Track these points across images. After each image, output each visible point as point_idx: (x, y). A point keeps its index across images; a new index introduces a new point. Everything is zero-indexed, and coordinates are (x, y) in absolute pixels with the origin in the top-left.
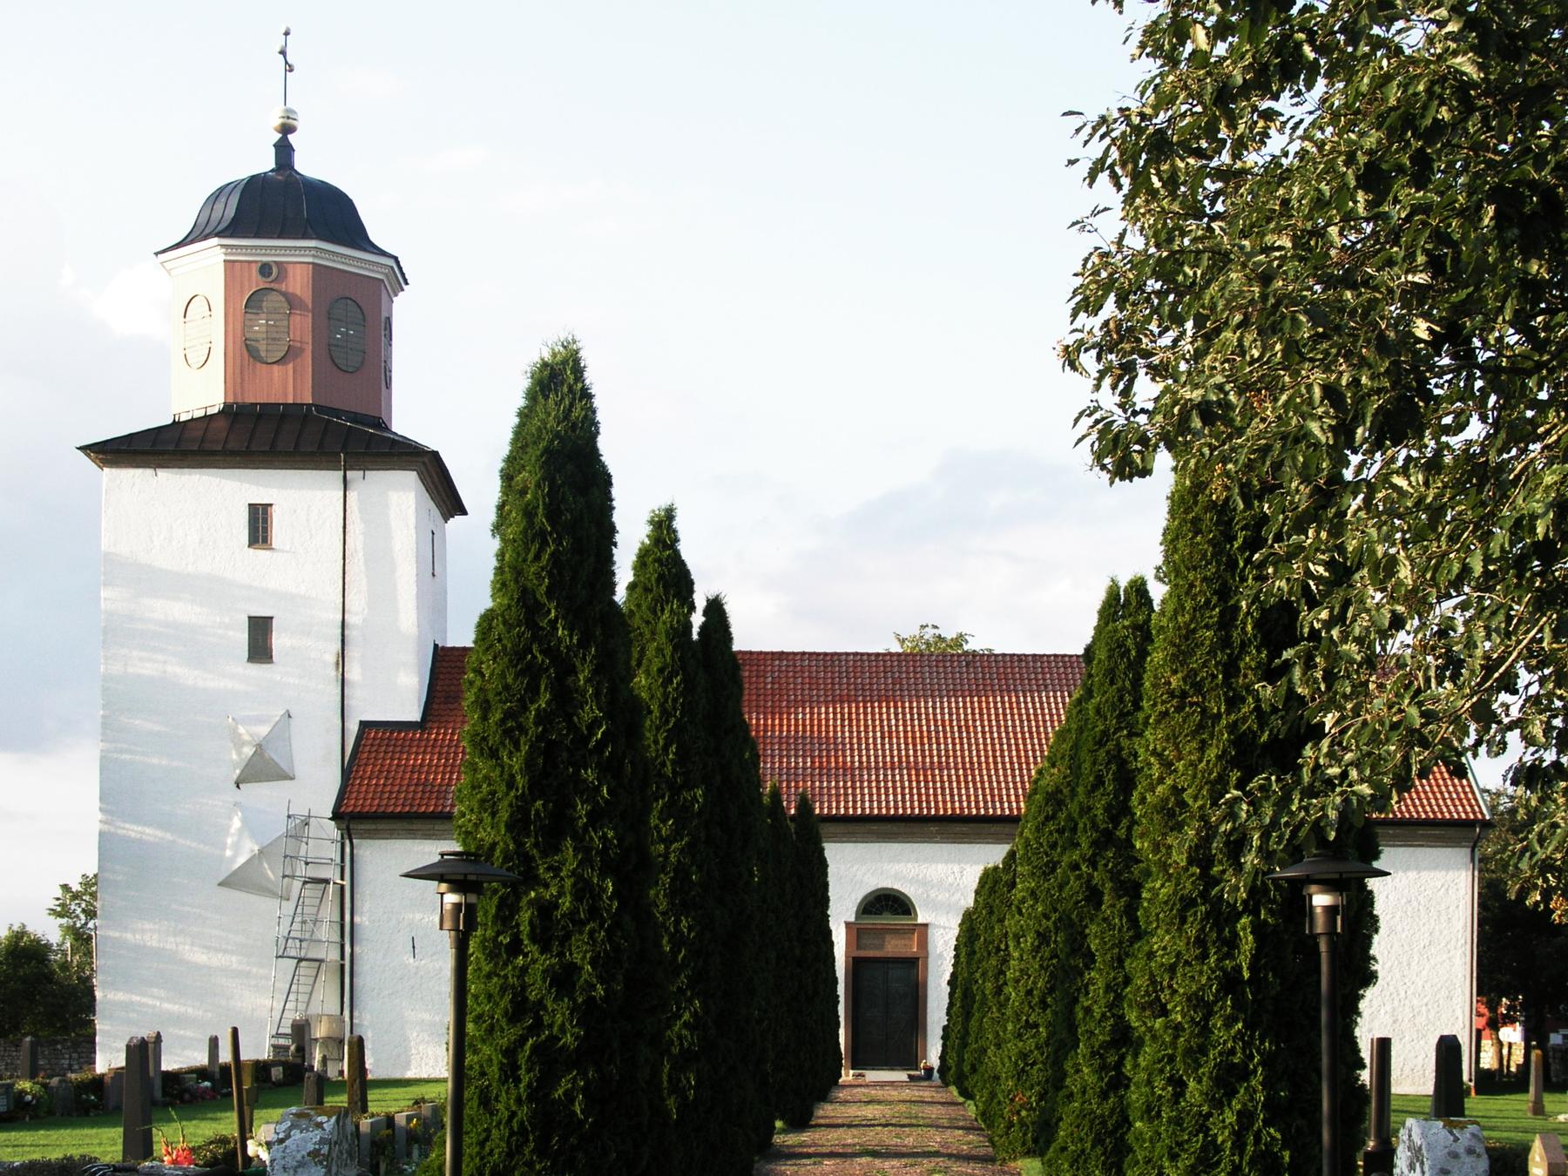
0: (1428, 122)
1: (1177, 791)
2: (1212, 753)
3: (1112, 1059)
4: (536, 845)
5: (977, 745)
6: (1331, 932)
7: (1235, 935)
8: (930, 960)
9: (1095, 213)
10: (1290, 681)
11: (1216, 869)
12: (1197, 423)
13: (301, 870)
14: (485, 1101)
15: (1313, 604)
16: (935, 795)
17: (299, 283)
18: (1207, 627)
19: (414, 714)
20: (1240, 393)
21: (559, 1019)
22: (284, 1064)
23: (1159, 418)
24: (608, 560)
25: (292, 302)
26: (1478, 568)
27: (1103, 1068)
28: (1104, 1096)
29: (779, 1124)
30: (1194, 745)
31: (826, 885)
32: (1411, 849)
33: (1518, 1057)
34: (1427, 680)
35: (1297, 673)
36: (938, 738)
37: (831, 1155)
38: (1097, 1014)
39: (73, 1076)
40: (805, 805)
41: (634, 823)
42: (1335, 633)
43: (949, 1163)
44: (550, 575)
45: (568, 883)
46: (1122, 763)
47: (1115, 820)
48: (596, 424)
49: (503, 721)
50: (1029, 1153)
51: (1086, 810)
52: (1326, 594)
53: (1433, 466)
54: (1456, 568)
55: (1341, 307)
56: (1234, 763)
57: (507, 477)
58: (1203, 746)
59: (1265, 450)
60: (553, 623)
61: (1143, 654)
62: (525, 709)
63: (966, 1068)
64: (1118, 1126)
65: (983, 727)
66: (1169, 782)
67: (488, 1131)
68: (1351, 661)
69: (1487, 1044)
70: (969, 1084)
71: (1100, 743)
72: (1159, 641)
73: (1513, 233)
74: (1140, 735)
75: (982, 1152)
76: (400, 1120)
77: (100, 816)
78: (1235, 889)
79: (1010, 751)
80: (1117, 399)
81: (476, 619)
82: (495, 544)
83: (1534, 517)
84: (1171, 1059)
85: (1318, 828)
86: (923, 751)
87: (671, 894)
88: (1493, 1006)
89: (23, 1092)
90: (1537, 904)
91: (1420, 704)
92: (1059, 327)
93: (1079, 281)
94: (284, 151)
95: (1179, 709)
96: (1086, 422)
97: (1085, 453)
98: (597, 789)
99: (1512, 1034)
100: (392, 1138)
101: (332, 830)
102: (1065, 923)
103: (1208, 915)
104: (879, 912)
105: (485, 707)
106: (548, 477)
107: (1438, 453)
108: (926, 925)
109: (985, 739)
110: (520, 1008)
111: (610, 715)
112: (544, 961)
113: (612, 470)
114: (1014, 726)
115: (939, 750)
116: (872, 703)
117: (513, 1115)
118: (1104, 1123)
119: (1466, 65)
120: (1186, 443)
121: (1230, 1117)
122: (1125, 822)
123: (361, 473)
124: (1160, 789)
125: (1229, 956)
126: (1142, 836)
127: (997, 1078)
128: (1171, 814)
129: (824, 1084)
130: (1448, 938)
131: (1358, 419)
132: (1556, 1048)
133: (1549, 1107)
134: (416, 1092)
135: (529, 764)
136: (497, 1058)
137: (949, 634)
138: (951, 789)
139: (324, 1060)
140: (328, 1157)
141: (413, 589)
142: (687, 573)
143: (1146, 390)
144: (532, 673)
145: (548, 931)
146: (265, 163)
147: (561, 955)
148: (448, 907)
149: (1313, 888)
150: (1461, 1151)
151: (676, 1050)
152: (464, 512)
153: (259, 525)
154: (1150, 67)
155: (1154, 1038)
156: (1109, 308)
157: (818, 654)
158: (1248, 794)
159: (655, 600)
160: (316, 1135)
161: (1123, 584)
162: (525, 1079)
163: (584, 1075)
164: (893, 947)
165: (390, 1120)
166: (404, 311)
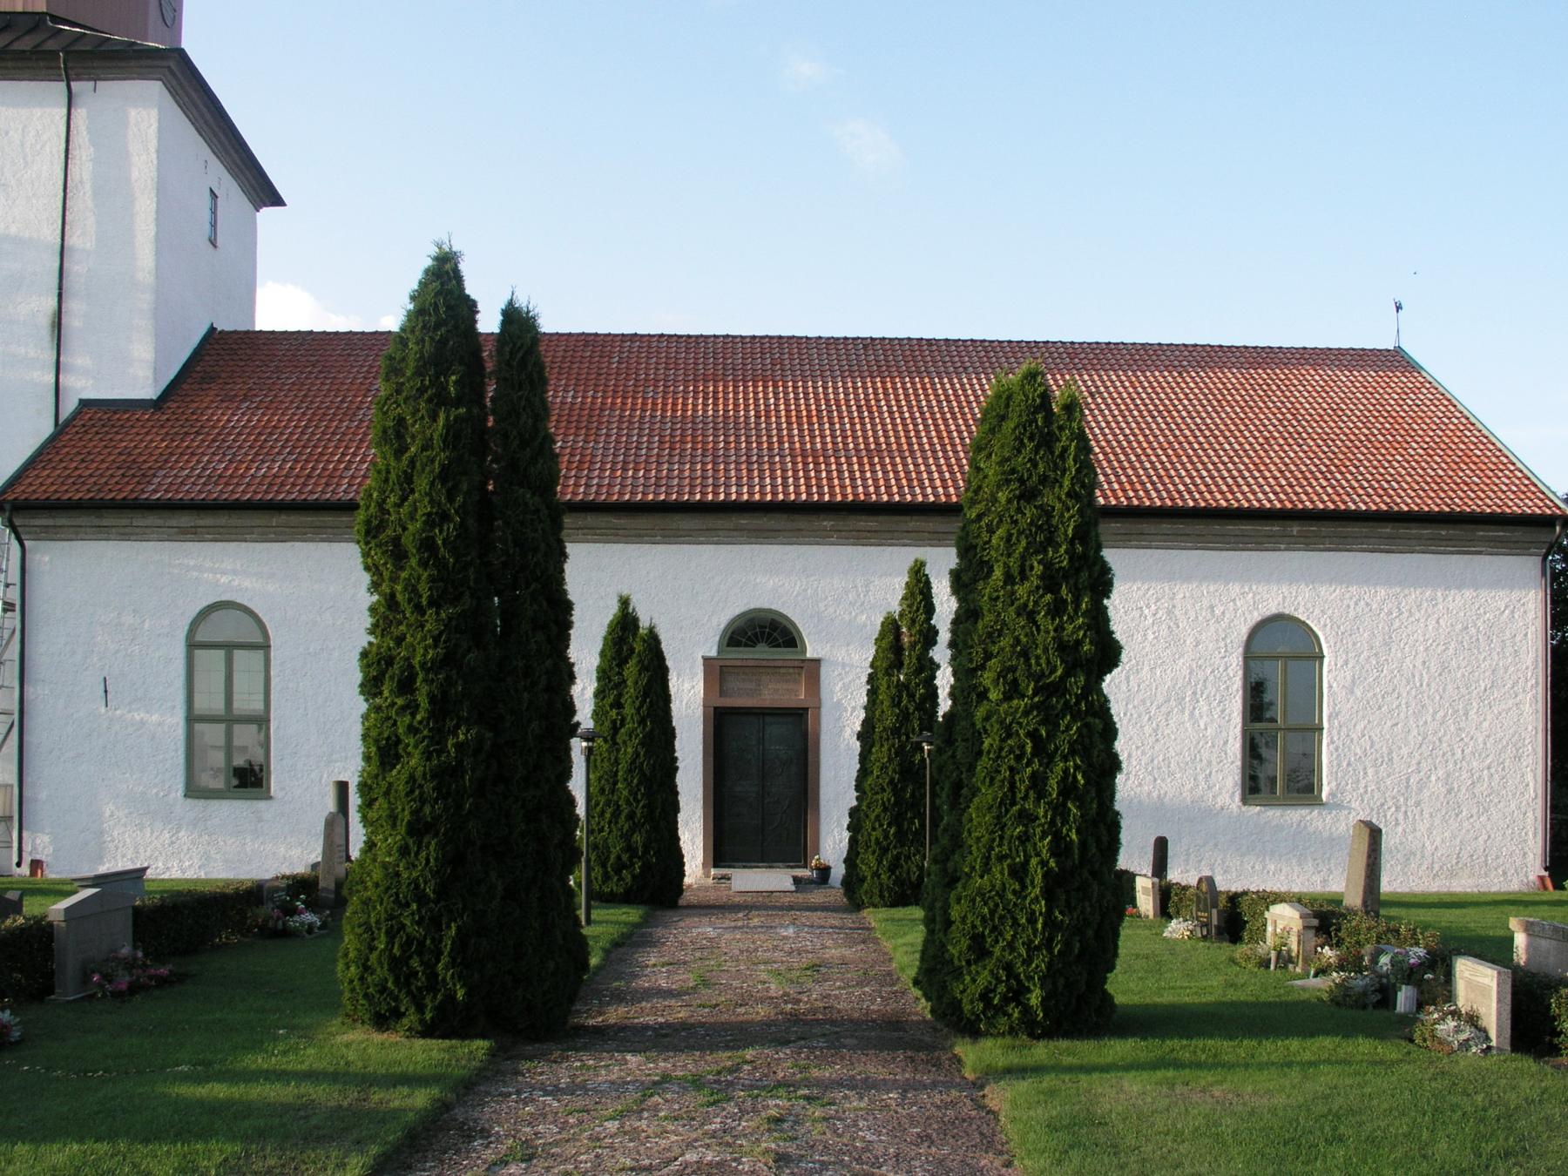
5: (884, 425)
8: (824, 711)
16: (830, 479)
32: (1467, 557)
36: (830, 418)
65: (890, 407)
79: (928, 432)
86: (811, 431)
104: (752, 642)
108: (817, 662)
109: (893, 419)
114: (930, 407)
115: (833, 431)
116: (745, 382)
123: (92, 83)
130: (1514, 677)
138: (851, 472)
152: (277, 201)
157: (681, 337)
164: (772, 694)
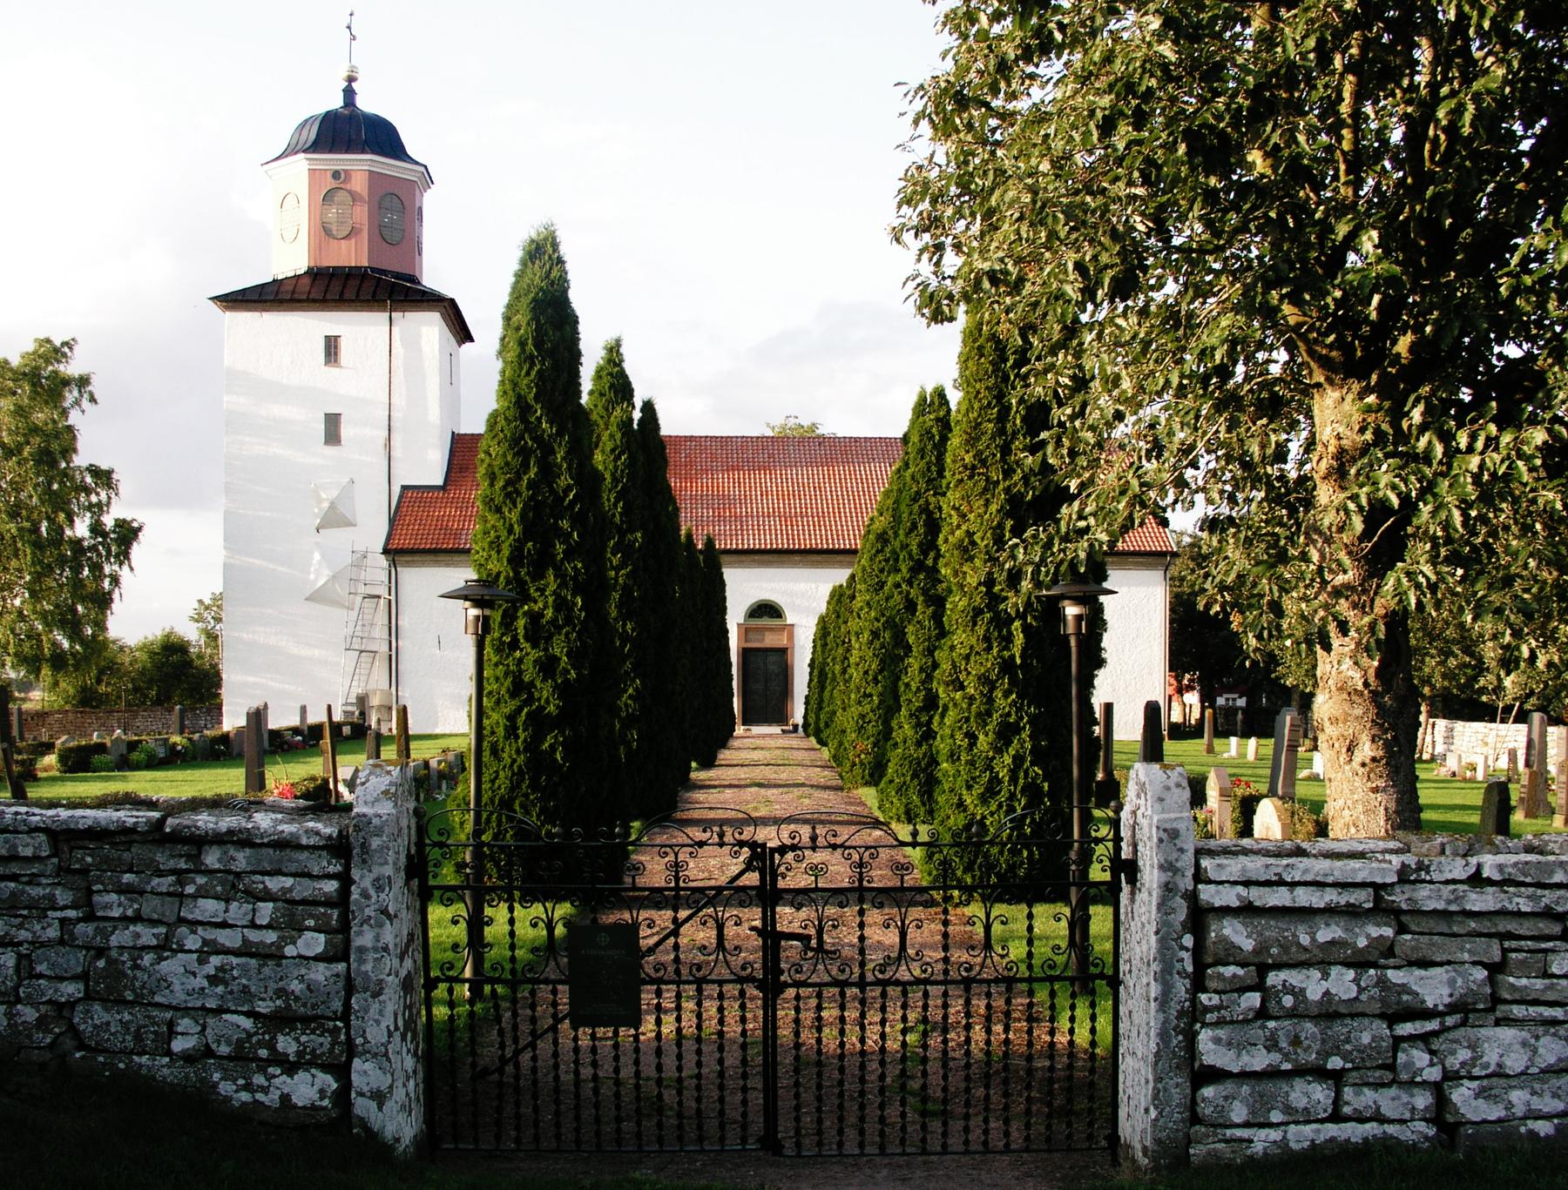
0: (1143, 88)
1: (970, 534)
2: (994, 508)
3: (924, 719)
4: (528, 573)
6: (1078, 633)
7: (1010, 633)
9: (912, 139)
10: (1045, 455)
11: (997, 588)
12: (986, 284)
13: (362, 590)
14: (495, 752)
15: (1061, 404)
17: (359, 184)
18: (989, 421)
19: (439, 481)
20: (1015, 264)
21: (545, 694)
22: (351, 724)
23: (960, 282)
24: (577, 375)
25: (354, 196)
26: (1175, 381)
27: (918, 725)
28: (919, 744)
29: (694, 765)
30: (982, 502)
31: (724, 599)
33: (1196, 714)
34: (1140, 458)
35: (1050, 449)
37: (730, 786)
38: (914, 686)
39: (207, 732)
40: (710, 542)
41: (595, 559)
42: (1077, 423)
43: (811, 791)
44: (537, 385)
45: (551, 599)
46: (930, 514)
47: (925, 554)
48: (566, 281)
49: (504, 487)
50: (867, 784)
51: (904, 546)
52: (1072, 397)
53: (1144, 312)
54: (1161, 382)
55: (1083, 206)
56: (1008, 515)
57: (507, 319)
58: (987, 504)
59: (1035, 305)
60: (539, 419)
61: (944, 439)
62: (520, 479)
63: (822, 725)
64: (929, 765)
66: (964, 527)
67: (497, 772)
68: (1087, 444)
69: (1176, 706)
70: (824, 736)
71: (915, 500)
72: (956, 430)
73: (1198, 160)
74: (944, 494)
75: (834, 783)
76: (433, 764)
77: (224, 552)
78: (1013, 602)
80: (932, 268)
81: (486, 417)
82: (499, 365)
83: (1214, 349)
84: (967, 720)
85: (1073, 565)
87: (619, 607)
88: (1179, 679)
89: (175, 744)
90: (1217, 613)
91: (1139, 477)
92: (889, 215)
93: (903, 183)
94: (349, 93)
95: (971, 477)
96: (913, 284)
97: (911, 306)
98: (570, 535)
99: (1192, 698)
100: (428, 777)
101: (383, 562)
102: (890, 624)
103: (991, 621)
104: (760, 616)
105: (492, 478)
106: (535, 318)
107: (1147, 305)
110: (519, 687)
111: (578, 482)
112: (534, 654)
113: (578, 313)
117: (514, 761)
118: (919, 764)
119: (1167, 50)
120: (980, 299)
121: (1008, 760)
122: (932, 554)
124: (958, 533)
125: (1007, 648)
126: (946, 565)
127: (844, 732)
128: (966, 550)
129: (724, 736)
131: (1099, 283)
132: (1221, 708)
133: (1217, 748)
134: (443, 743)
135: (523, 517)
136: (503, 722)
137: (806, 423)
139: (379, 721)
140: (395, 795)
141: (438, 394)
142: (629, 384)
143: (952, 261)
144: (524, 453)
145: (537, 633)
146: (336, 102)
147: (546, 650)
148: (470, 618)
149: (1066, 602)
150: (1172, 785)
151: (624, 714)
152: (472, 340)
153: (332, 348)
154: (949, 40)
155: (955, 705)
156: (925, 205)
158: (1023, 541)
159: (609, 402)
160: (387, 780)
161: (929, 390)
162: (522, 736)
163: (562, 732)
164: (771, 641)
165: (426, 764)
166: (430, 202)
